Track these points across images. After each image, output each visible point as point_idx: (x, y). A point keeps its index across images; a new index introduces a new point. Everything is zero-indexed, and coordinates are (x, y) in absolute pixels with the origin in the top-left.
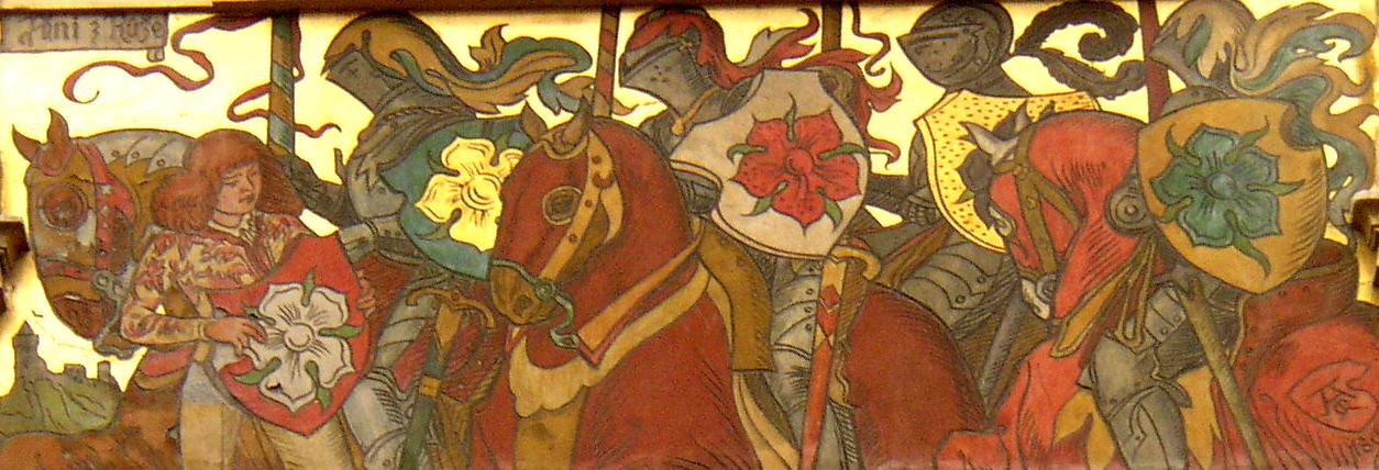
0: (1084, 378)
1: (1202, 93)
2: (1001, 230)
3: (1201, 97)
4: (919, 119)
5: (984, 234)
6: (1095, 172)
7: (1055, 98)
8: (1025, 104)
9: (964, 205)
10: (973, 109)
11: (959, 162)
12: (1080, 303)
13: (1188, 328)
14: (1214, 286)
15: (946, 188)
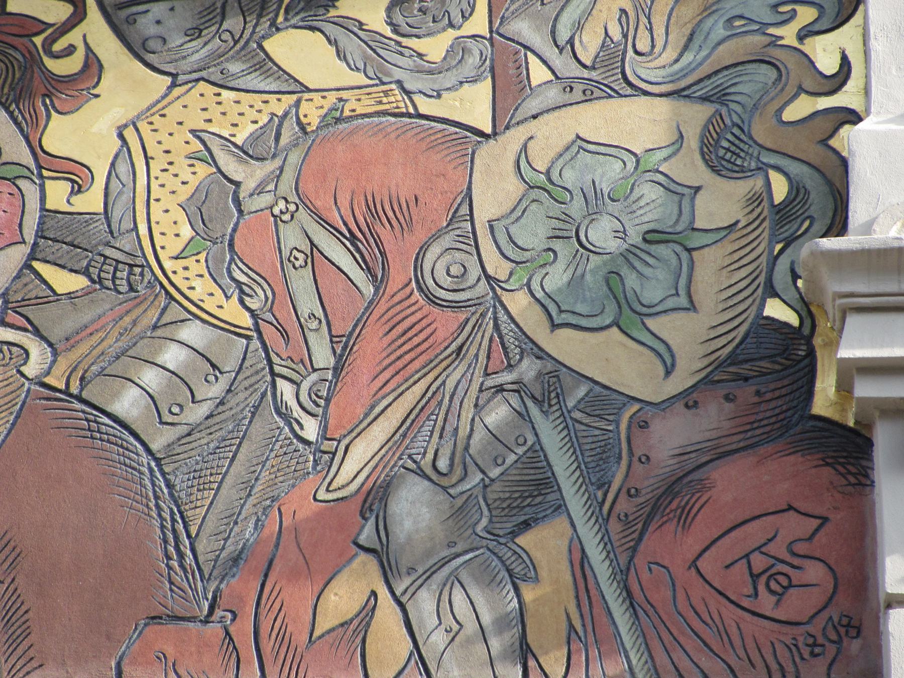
0: (367, 535)
1: (578, 88)
2: (247, 300)
3: (577, 95)
4: (126, 126)
5: (221, 307)
6: (401, 215)
7: (344, 95)
8: (298, 103)
9: (190, 262)
10: (214, 112)
11: (184, 193)
12: (370, 417)
13: (536, 456)
14: (582, 391)
15: (163, 234)
